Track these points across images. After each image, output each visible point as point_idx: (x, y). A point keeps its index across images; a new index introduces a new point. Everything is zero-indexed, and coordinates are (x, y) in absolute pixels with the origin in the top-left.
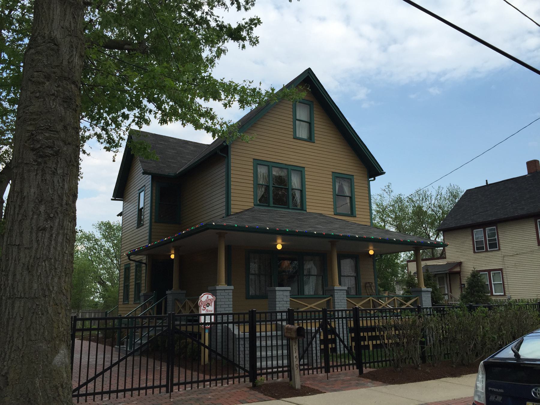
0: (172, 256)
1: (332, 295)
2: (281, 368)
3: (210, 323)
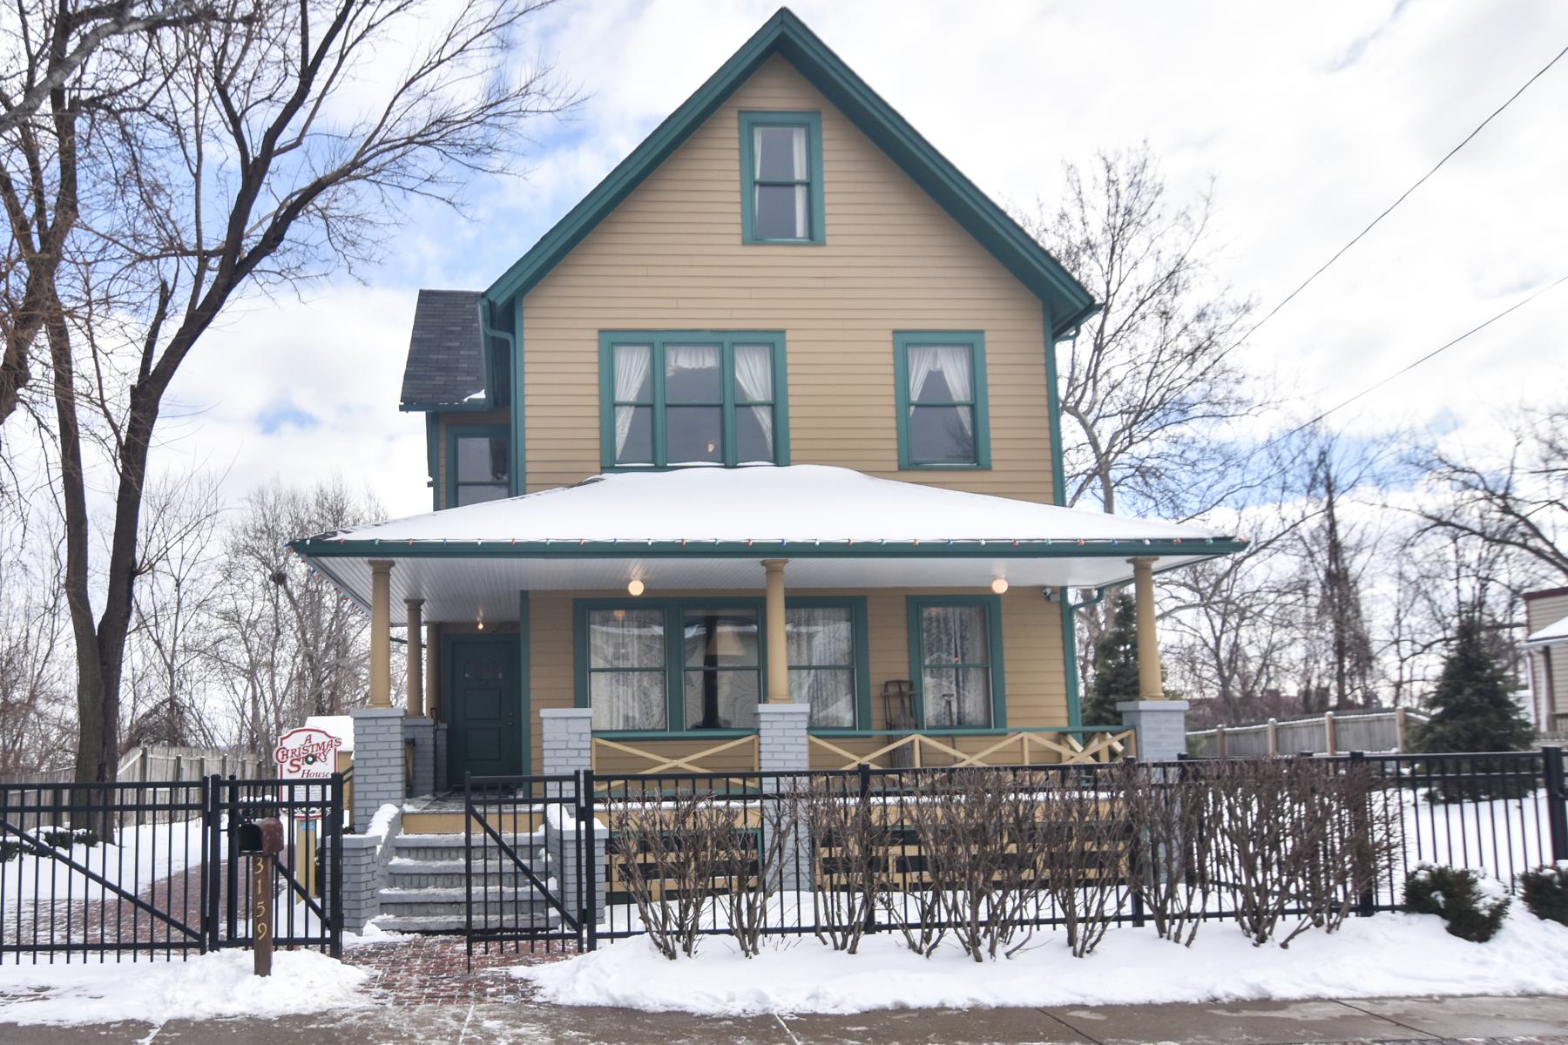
1: (1134, 728)
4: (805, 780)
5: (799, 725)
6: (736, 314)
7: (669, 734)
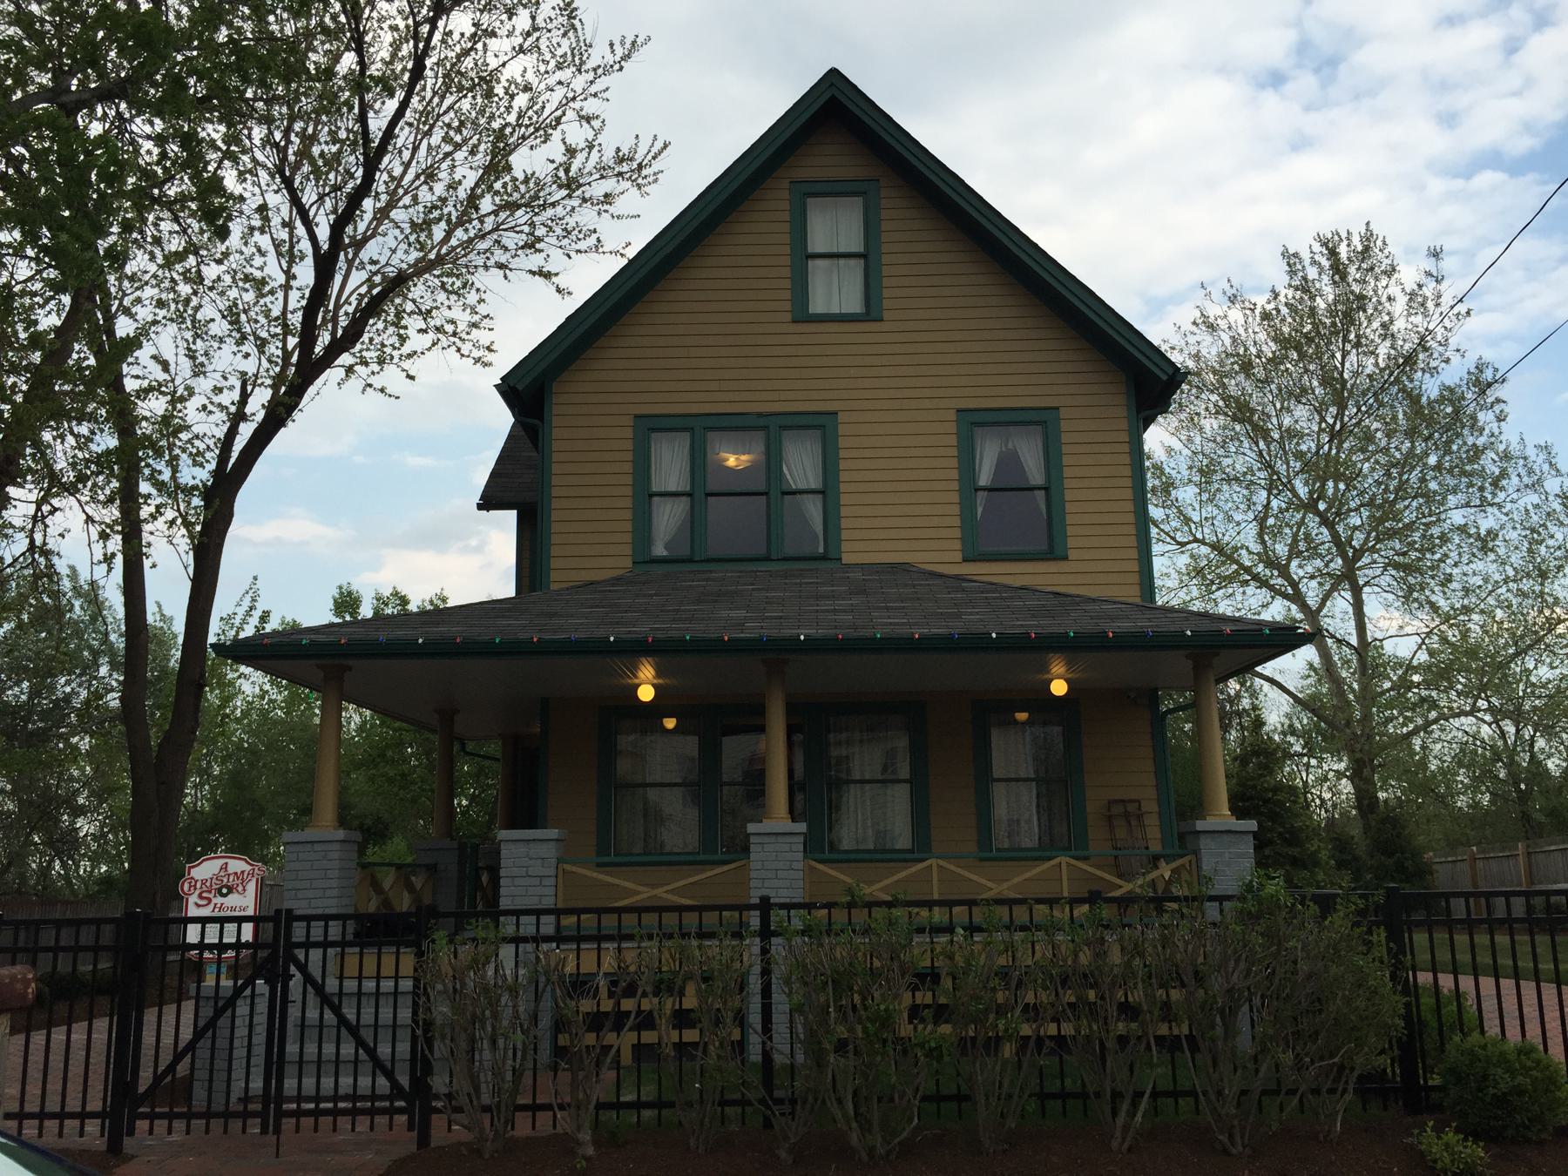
2: (311, 1102)
3: (238, 946)
4: (551, 919)
5: (794, 848)
7: (702, 857)
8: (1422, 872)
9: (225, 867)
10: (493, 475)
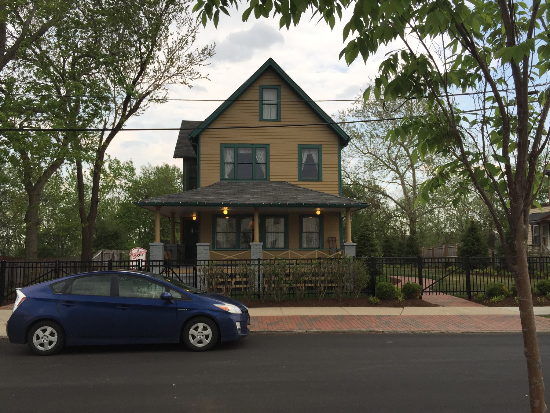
0: (194, 218)
6: (257, 140)
8: (418, 252)
9: (138, 250)
10: (176, 148)
